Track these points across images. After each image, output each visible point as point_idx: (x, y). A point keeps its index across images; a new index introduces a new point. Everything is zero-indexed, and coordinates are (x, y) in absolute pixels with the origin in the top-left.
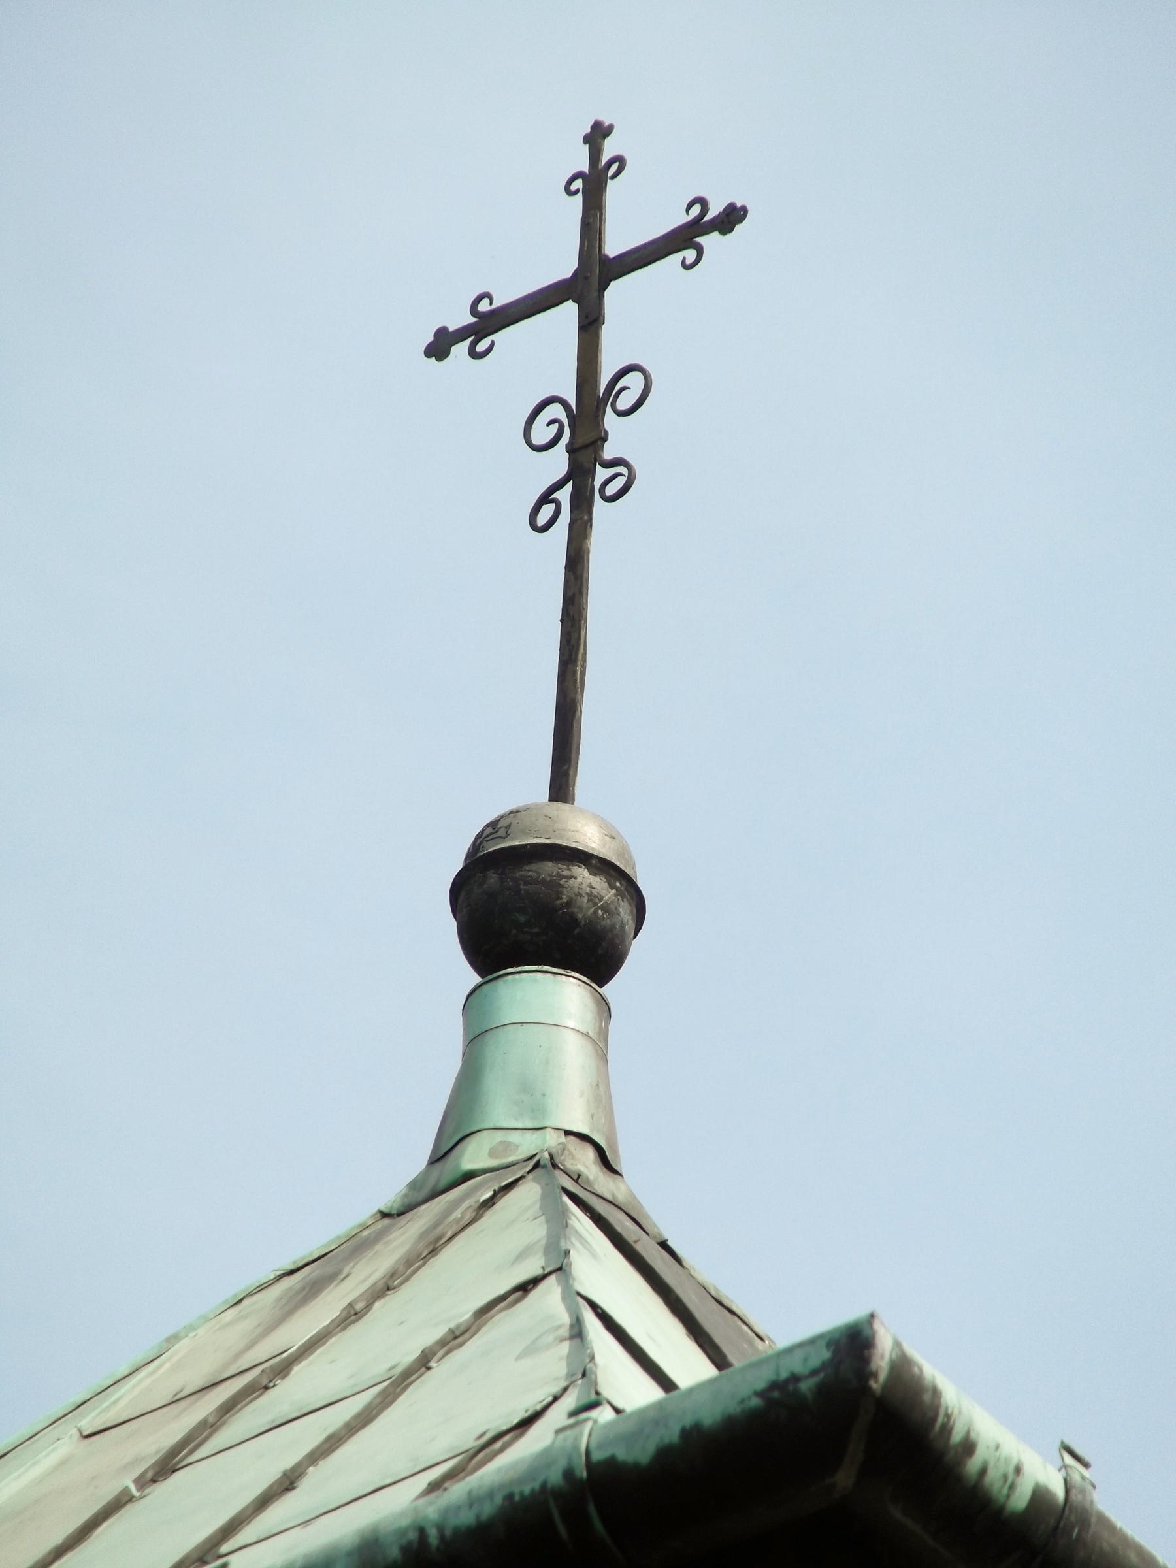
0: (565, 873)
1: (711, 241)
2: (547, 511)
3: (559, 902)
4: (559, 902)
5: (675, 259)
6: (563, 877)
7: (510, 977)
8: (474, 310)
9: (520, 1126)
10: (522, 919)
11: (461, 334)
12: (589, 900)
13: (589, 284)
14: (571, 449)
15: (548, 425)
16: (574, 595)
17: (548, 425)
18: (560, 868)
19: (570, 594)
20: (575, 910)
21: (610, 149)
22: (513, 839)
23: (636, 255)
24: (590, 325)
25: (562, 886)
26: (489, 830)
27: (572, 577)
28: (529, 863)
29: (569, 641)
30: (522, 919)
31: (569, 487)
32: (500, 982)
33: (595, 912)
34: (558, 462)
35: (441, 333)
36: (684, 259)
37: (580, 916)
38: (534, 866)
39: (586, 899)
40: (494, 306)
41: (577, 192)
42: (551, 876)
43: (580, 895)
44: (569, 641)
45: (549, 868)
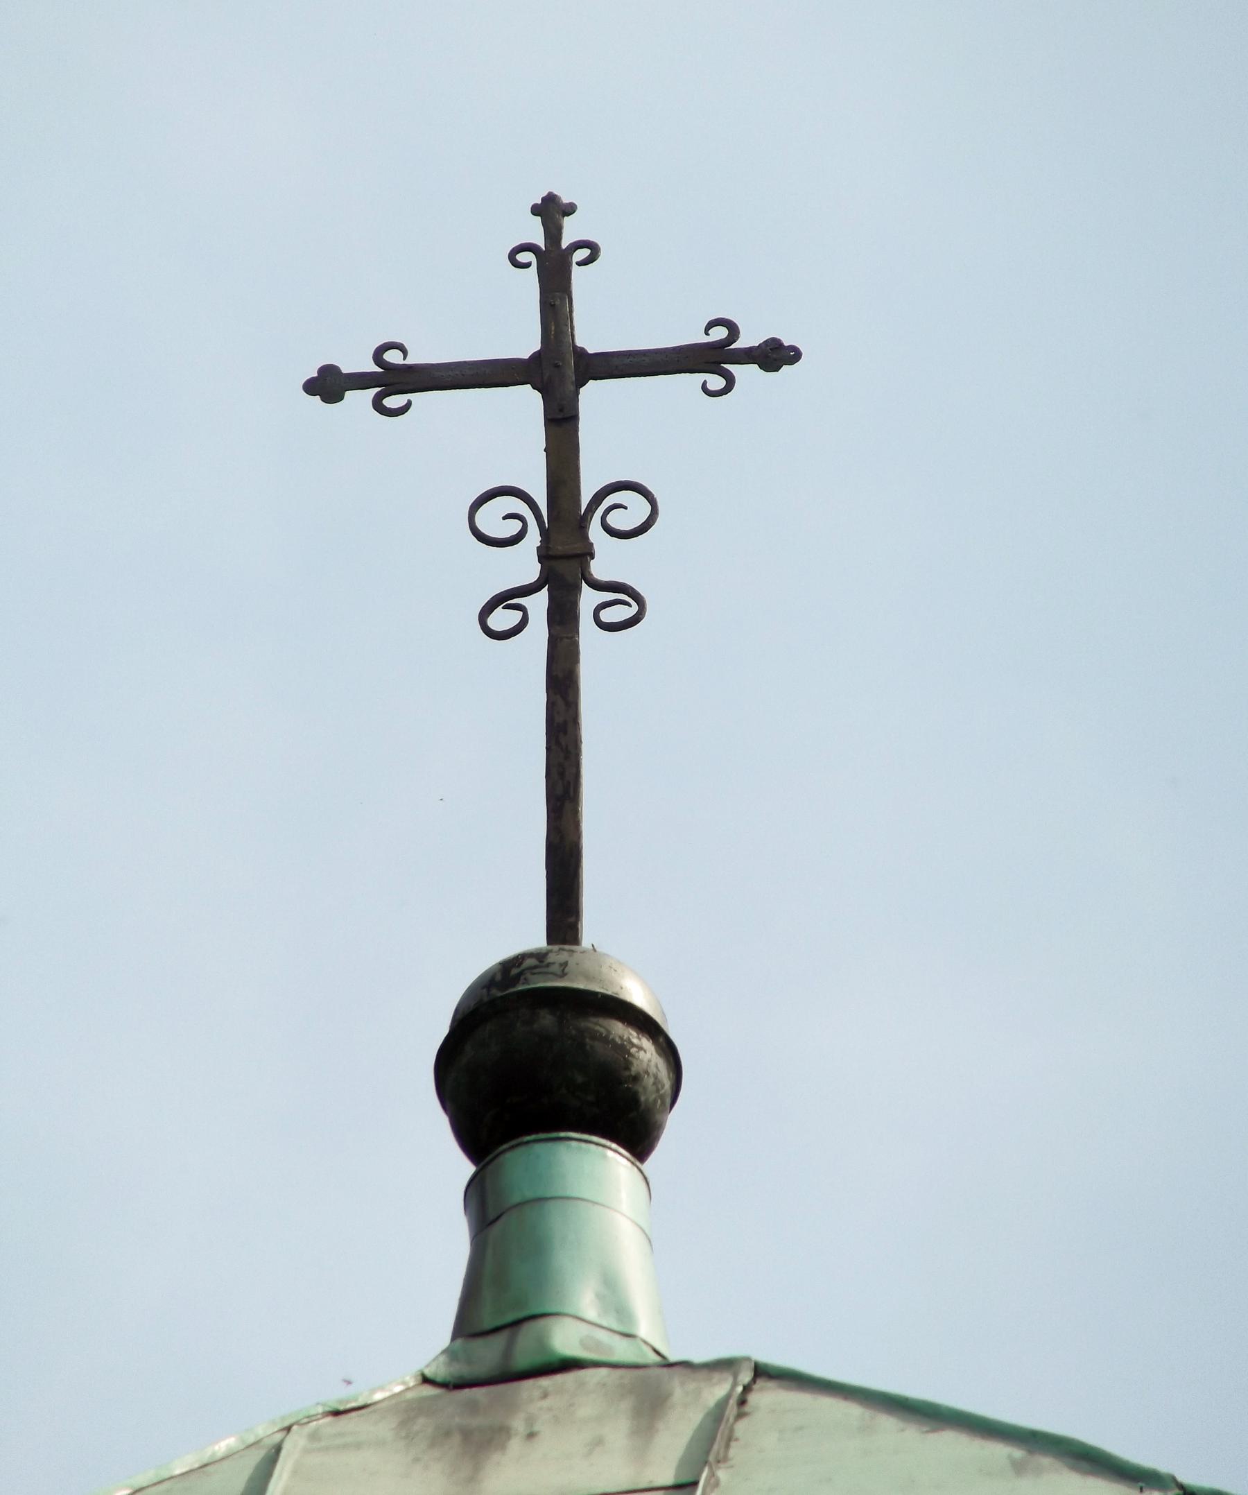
0: (635, 1041)
1: (745, 373)
2: (502, 619)
3: (627, 1073)
4: (627, 1073)
5: (693, 381)
6: (633, 1045)
7: (574, 1144)
8: (378, 356)
9: (605, 1323)
10: (580, 1079)
11: (360, 381)
12: (654, 1084)
13: (558, 372)
14: (544, 555)
15: (504, 518)
16: (565, 723)
17: (504, 518)
18: (633, 1035)
19: (559, 719)
20: (640, 1090)
21: (572, 231)
22: (572, 981)
23: (627, 361)
24: (562, 424)
25: (632, 1056)
26: (530, 962)
27: (560, 702)
28: (595, 1015)
29: (562, 775)
30: (580, 1079)
31: (543, 595)
32: (501, 1158)
33: (655, 1101)
34: (523, 564)
35: (329, 372)
36: (705, 383)
37: (643, 1098)
38: (602, 1021)
39: (652, 1080)
40: (406, 362)
41: (527, 265)
42: (621, 1038)
43: (647, 1072)
44: (562, 775)
45: (620, 1030)
